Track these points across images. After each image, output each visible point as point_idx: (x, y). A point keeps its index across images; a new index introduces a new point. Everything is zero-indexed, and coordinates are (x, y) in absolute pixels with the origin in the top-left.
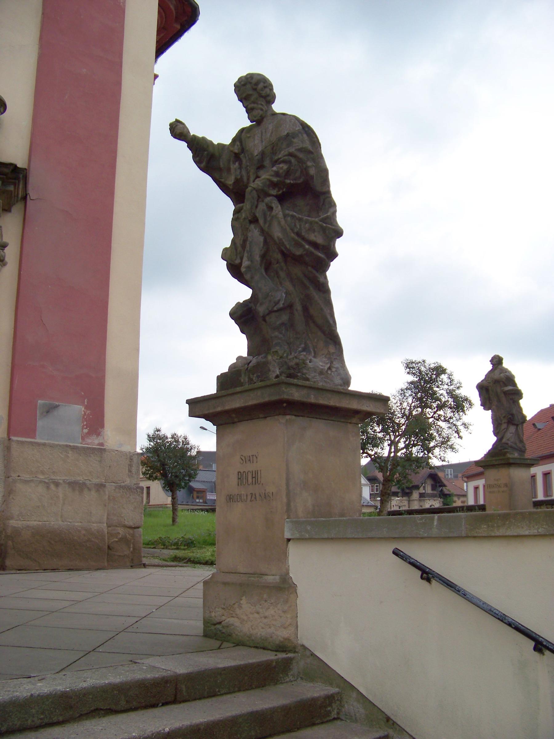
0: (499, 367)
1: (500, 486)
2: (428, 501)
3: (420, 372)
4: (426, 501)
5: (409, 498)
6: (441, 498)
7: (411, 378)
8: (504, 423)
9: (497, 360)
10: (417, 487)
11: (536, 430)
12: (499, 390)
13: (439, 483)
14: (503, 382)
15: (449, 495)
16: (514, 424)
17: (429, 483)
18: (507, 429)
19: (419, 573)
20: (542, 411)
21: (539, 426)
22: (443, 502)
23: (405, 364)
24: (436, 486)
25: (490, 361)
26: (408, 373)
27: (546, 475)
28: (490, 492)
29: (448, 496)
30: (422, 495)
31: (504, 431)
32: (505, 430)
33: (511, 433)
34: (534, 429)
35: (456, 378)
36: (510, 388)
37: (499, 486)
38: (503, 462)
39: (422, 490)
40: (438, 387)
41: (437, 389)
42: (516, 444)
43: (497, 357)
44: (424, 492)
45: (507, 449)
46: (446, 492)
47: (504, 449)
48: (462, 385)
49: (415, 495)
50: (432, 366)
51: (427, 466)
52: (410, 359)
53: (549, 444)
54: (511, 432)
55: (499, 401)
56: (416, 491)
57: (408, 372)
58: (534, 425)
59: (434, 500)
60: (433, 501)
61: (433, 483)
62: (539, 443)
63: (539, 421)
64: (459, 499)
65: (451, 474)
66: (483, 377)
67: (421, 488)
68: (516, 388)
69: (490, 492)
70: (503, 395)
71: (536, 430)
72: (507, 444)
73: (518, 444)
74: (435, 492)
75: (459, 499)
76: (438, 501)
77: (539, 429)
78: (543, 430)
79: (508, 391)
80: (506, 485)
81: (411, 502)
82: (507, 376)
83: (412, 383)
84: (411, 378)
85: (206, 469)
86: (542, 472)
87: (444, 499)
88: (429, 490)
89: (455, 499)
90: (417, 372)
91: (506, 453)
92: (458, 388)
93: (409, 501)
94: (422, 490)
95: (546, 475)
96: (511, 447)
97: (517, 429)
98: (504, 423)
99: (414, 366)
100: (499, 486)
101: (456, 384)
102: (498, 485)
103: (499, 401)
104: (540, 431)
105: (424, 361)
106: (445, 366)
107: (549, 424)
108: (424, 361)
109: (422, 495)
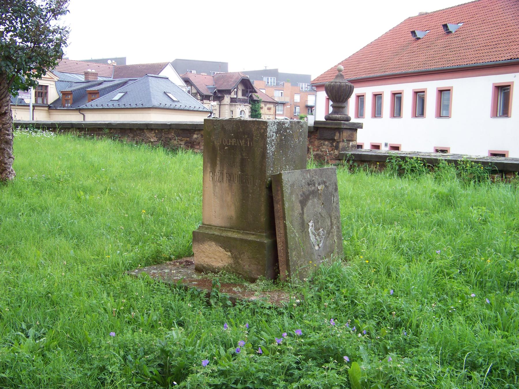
2: (239, 106)
4: (237, 106)
5: (220, 102)
6: (250, 103)
10: (229, 92)
11: (414, 38)
13: (250, 89)
15: (258, 101)
17: (241, 88)
19: (69, 59)
20: (410, 19)
22: (251, 108)
24: (247, 92)
29: (256, 102)
30: (233, 100)
34: (412, 37)
39: (233, 95)
44: (235, 96)
46: (255, 98)
49: (227, 99)
56: (227, 96)
59: (245, 106)
60: (244, 106)
61: (244, 88)
64: (265, 105)
65: (274, 82)
67: (233, 93)
74: (245, 98)
75: (265, 105)
76: (248, 107)
77: (419, 39)
81: (222, 106)
85: (377, 108)
86: (413, 90)
87: (252, 105)
88: (240, 96)
89: (262, 105)
93: (220, 105)
94: (233, 95)
104: (420, 40)
109: (233, 100)
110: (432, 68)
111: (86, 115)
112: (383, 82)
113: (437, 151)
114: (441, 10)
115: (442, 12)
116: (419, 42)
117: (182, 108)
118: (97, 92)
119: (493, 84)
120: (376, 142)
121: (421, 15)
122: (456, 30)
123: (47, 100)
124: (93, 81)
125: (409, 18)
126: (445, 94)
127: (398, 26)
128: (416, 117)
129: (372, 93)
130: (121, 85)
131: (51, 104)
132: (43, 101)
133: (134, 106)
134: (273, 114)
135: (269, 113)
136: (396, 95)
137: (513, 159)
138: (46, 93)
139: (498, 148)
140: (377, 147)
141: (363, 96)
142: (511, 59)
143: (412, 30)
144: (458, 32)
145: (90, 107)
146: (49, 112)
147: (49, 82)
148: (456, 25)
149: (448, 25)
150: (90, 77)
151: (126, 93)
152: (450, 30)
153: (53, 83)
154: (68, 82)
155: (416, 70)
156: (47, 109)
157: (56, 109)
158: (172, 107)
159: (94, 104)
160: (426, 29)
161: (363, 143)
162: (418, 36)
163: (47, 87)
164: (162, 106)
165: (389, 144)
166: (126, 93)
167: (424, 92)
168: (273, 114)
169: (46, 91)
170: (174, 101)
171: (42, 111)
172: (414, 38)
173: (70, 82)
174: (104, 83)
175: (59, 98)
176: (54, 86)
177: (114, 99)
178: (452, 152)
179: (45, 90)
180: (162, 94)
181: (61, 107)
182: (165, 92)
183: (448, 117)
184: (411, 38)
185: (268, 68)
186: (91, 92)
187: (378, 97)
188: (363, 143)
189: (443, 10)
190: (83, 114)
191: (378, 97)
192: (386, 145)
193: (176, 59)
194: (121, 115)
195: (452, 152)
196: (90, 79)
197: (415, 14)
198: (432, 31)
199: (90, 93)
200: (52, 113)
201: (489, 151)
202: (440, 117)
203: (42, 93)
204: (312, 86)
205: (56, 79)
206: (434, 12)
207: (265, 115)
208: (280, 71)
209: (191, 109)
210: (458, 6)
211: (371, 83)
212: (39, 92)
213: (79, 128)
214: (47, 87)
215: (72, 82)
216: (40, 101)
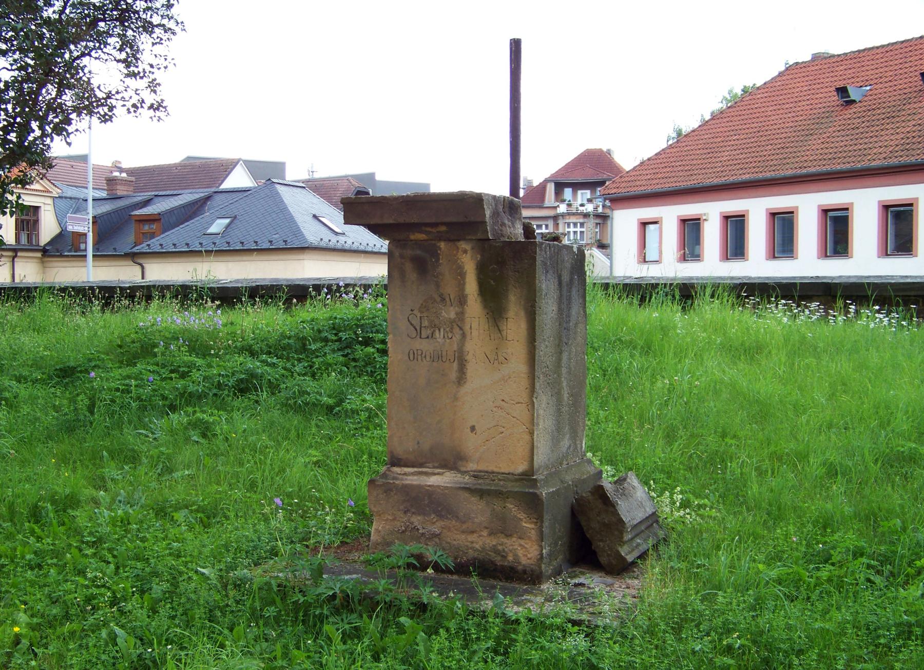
11: (841, 102)
111: (147, 266)
112: (785, 189)
114: (878, 48)
115: (883, 50)
116: (853, 109)
117: (356, 248)
118: (157, 217)
121: (816, 58)
123: (38, 236)
124: (128, 196)
128: (887, 255)
129: (721, 213)
130: (140, 205)
131: (46, 245)
132: (29, 238)
133: (266, 245)
136: (831, 214)
138: (36, 222)
143: (840, 84)
145: (158, 249)
146: (43, 262)
147: (42, 200)
150: (118, 187)
151: (235, 217)
153: (50, 201)
154: (71, 198)
156: (39, 255)
157: (61, 256)
158: (331, 245)
159: (167, 240)
162: (852, 98)
163: (36, 209)
164: (323, 244)
166: (235, 217)
167: (792, 212)
169: (35, 218)
170: (336, 233)
171: (29, 260)
172: (841, 102)
173: (75, 198)
174: (156, 200)
175: (61, 232)
176: (51, 208)
177: (210, 231)
179: (34, 215)
180: (310, 218)
181: (70, 251)
182: (315, 217)
184: (835, 98)
185: (317, 176)
186: (141, 218)
189: (883, 46)
190: (141, 265)
193: (189, 158)
194: (231, 265)
196: (119, 193)
199: (140, 221)
200: (47, 265)
203: (28, 221)
204: (605, 199)
205: (55, 192)
206: (859, 51)
208: (378, 178)
209: (370, 249)
211: (761, 191)
212: (23, 221)
214: (36, 209)
215: (78, 199)
216: (24, 240)
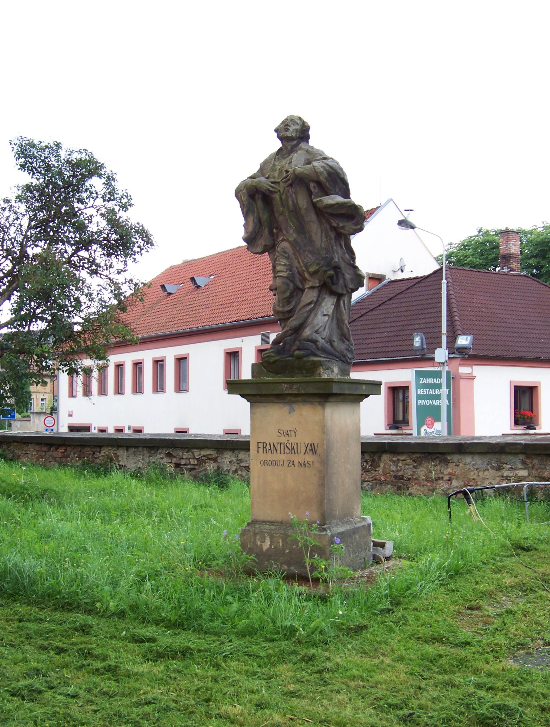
0: (303, 145)
1: (293, 448)
3: (48, 168)
7: (26, 178)
8: (312, 288)
9: (298, 127)
11: (165, 294)
12: (303, 202)
14: (319, 183)
16: (333, 293)
18: (317, 303)
20: (172, 268)
21: (170, 288)
23: (16, 147)
25: (276, 131)
26: (23, 167)
27: (181, 361)
28: (265, 463)
31: (308, 308)
32: (313, 305)
33: (324, 315)
34: (162, 292)
35: (120, 186)
36: (339, 199)
37: (293, 450)
38: (311, 390)
40: (81, 201)
41: (81, 206)
42: (331, 342)
43: (298, 121)
45: (315, 355)
47: (308, 356)
48: (132, 202)
50: (75, 156)
51: (61, 367)
52: (29, 138)
53: (187, 317)
54: (325, 313)
55: (302, 229)
57: (21, 165)
58: (163, 287)
62: (170, 313)
63: (169, 282)
66: (254, 169)
68: (350, 202)
69: (265, 463)
70: (313, 216)
71: (165, 294)
72: (315, 342)
73: (335, 344)
78: (175, 295)
79: (332, 206)
80: (312, 449)
82: (331, 167)
83: (28, 188)
84: (26, 178)
90: (39, 167)
91: (316, 366)
92: (124, 207)
95: (181, 361)
96: (324, 350)
97: (337, 306)
98: (312, 288)
99: (36, 154)
100: (293, 450)
101: (120, 199)
102: (290, 447)
103: (302, 229)
105: (58, 145)
106: (99, 158)
107: (184, 287)
108: (58, 145)
110: (167, 332)
112: (231, 334)
113: (375, 434)
119: (225, 350)
120: (120, 425)
122: (205, 284)
125: (171, 266)
126: (138, 366)
127: (157, 277)
134: (49, 391)
135: (43, 391)
137: (196, 435)
139: (181, 426)
140: (120, 430)
141: (163, 361)
142: (235, 321)
144: (207, 287)
148: (207, 278)
149: (195, 278)
152: (199, 284)
155: (159, 333)
160: (180, 282)
161: (107, 427)
162: (169, 291)
165: (98, 427)
168: (49, 391)
178: (191, 432)
183: (186, 391)
187: (159, 364)
188: (107, 427)
191: (159, 364)
192: (129, 428)
195: (191, 432)
197: (178, 261)
198: (186, 284)
201: (224, 430)
202: (180, 391)
207: (38, 394)
210: (237, 248)
211: (219, 335)
213: (47, 444)
